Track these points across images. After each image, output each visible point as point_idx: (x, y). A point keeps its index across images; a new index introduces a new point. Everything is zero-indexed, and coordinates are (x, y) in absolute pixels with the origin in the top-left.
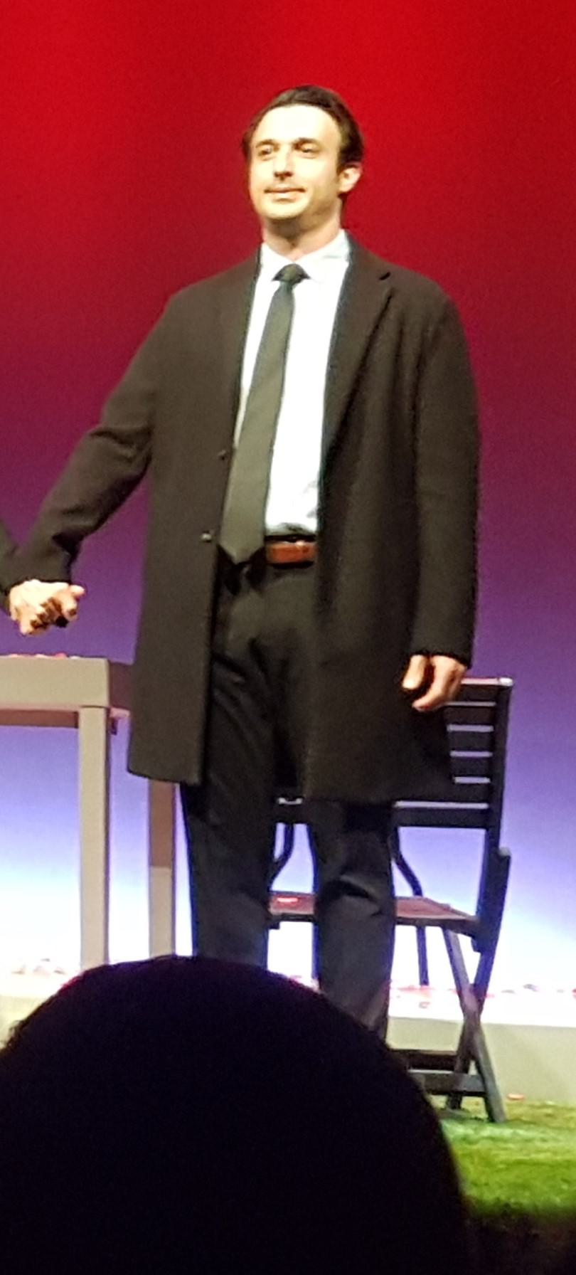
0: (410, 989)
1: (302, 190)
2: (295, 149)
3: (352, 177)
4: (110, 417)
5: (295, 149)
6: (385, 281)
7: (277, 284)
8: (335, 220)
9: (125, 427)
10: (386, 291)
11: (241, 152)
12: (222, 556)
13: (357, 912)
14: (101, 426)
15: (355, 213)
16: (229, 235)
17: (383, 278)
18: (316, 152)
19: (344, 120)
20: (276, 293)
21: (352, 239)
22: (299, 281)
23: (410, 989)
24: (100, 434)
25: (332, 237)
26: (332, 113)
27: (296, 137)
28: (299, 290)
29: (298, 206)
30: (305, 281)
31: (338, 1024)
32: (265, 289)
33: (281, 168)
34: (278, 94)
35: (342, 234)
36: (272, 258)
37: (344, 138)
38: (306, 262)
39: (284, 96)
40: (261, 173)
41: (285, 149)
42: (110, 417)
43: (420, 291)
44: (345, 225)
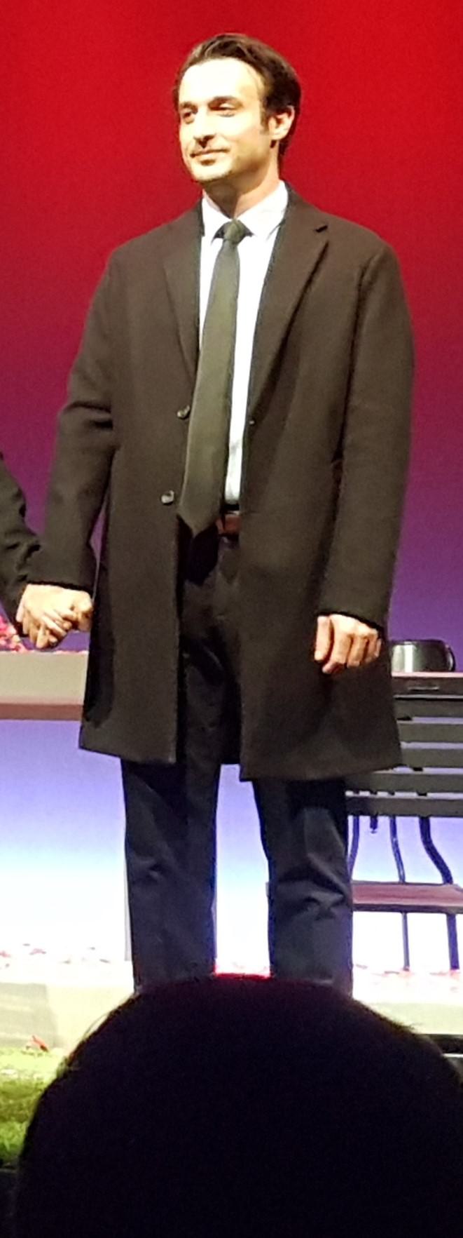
0: (441, 974)
1: (225, 151)
2: (221, 103)
3: (281, 129)
4: (76, 389)
5: (221, 103)
6: (319, 235)
7: (219, 241)
8: (272, 169)
9: (94, 397)
10: (321, 245)
11: (172, 113)
12: (183, 528)
13: (309, 899)
14: (70, 401)
15: (291, 159)
16: (170, 196)
17: (320, 230)
18: (239, 106)
19: (264, 69)
20: (221, 252)
21: (287, 186)
22: (242, 238)
23: (441, 974)
24: (76, 405)
25: (272, 188)
26: (249, 62)
27: (211, 96)
28: (244, 246)
29: (222, 167)
30: (247, 239)
31: (307, 1003)
32: (210, 249)
33: (201, 134)
34: (188, 49)
35: (282, 184)
36: (213, 217)
37: (265, 84)
38: (245, 219)
39: (197, 51)
40: (188, 135)
41: (203, 110)
42: (76, 389)
43: (357, 244)
44: (281, 178)
